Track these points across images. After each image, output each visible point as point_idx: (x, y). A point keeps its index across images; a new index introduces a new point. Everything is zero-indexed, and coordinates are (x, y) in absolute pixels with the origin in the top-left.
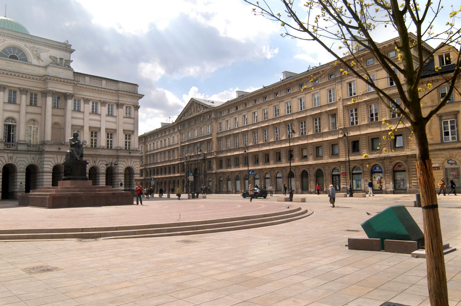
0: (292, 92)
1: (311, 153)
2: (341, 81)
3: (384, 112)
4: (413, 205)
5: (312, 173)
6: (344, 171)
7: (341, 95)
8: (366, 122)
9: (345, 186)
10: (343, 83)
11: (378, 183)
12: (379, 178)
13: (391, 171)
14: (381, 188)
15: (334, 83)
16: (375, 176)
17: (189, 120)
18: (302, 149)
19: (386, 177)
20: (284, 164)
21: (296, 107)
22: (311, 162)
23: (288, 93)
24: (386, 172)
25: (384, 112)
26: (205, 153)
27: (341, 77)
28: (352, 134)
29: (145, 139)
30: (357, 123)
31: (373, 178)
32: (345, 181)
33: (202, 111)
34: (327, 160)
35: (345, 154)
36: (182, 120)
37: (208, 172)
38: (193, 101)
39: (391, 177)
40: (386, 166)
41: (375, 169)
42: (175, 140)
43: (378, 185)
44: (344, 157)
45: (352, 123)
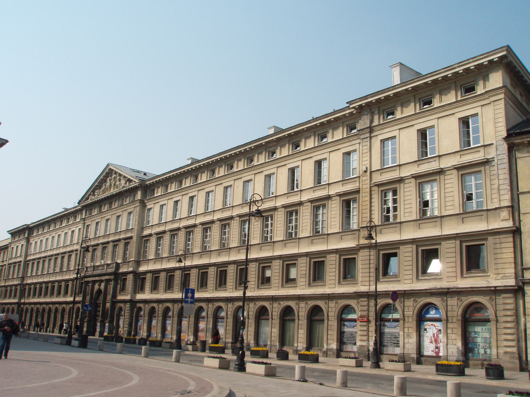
0: (330, 140)
1: (304, 272)
2: (371, 138)
3: (450, 199)
4: (263, 373)
5: (302, 310)
6: (365, 313)
7: (368, 162)
8: (281, 238)
9: (365, 344)
10: (373, 140)
11: (431, 342)
12: (435, 331)
13: (460, 318)
14: (437, 353)
15: (358, 141)
16: (426, 327)
17: (100, 203)
18: (288, 266)
19: (449, 331)
20: (231, 292)
21: (216, 202)
22: (302, 289)
23: (231, 171)
24: (450, 320)
25: (450, 199)
26: (119, 261)
27: (371, 129)
28: (381, 239)
29: (144, 195)
30: (395, 217)
31: (422, 330)
32: (365, 333)
33: (123, 185)
34: (331, 286)
35: (368, 279)
36: (89, 201)
37: (120, 298)
38: (110, 169)
39: (459, 332)
40: (449, 308)
41: (427, 312)
42: (68, 238)
43: (432, 346)
44: (367, 283)
45: (387, 218)
